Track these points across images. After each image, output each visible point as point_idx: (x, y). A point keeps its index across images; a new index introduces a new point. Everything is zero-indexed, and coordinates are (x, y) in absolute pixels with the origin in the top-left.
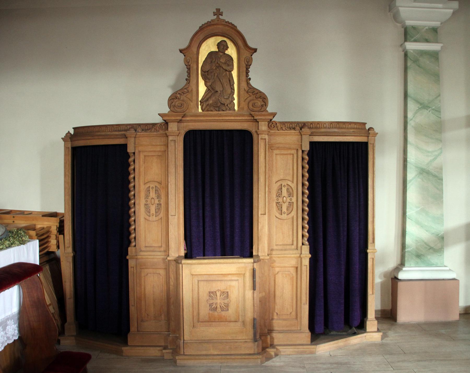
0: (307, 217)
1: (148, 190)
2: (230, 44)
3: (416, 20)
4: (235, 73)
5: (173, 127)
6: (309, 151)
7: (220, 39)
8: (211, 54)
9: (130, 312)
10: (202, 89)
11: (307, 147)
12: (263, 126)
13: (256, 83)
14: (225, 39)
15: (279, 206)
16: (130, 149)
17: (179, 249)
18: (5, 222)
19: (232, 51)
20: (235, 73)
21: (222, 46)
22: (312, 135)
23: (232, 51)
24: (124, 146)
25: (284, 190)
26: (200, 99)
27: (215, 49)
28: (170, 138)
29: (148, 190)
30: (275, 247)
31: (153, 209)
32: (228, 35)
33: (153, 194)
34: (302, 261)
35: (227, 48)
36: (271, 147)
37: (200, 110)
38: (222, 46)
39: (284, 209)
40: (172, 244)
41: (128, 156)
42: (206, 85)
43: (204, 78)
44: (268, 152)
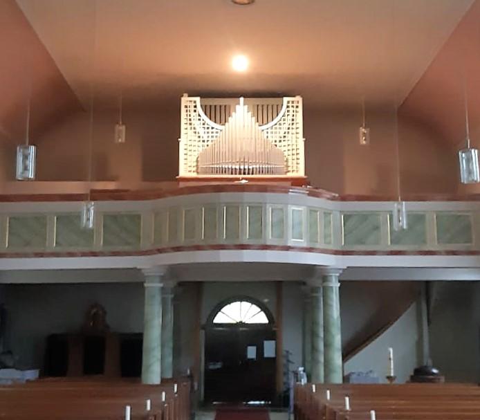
23: (101, 312)
34: (359, 252)
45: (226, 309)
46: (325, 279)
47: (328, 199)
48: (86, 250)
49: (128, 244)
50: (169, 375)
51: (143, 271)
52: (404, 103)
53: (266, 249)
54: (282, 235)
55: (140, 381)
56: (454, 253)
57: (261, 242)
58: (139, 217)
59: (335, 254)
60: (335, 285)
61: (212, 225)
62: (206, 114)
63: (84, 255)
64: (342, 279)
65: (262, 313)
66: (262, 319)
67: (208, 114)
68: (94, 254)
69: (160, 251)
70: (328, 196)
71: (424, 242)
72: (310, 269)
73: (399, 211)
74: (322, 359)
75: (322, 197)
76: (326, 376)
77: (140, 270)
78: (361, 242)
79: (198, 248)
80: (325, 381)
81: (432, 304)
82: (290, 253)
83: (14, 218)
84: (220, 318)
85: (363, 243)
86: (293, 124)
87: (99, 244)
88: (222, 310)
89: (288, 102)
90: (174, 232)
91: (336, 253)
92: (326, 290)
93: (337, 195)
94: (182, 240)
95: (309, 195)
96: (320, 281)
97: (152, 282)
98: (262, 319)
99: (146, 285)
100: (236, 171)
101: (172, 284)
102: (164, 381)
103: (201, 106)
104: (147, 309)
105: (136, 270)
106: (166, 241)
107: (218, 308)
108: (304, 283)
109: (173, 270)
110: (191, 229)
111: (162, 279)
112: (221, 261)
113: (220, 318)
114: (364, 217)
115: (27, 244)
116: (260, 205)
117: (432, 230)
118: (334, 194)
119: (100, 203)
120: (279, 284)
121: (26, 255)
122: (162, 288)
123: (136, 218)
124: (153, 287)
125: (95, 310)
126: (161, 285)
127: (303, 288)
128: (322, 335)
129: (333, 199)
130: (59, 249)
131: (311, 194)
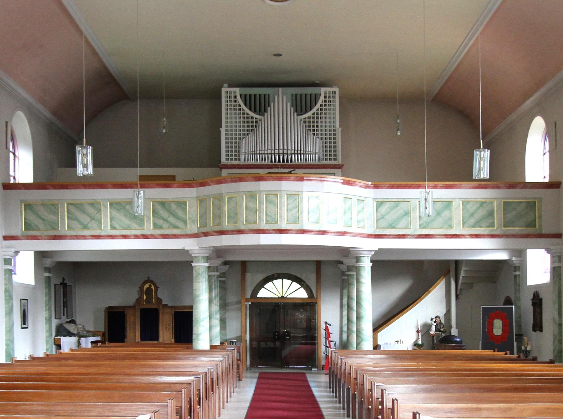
1: (166, 324)
2: (152, 285)
4: (153, 293)
5: (137, 307)
7: (150, 284)
8: (147, 288)
9: (140, 327)
10: (145, 297)
12: (161, 307)
13: (159, 296)
16: (126, 313)
18: (322, 298)
19: (153, 287)
20: (153, 293)
21: (150, 286)
22: (175, 309)
23: (153, 287)
24: (124, 312)
27: (148, 287)
29: (166, 324)
31: (132, 329)
33: (131, 325)
35: (151, 286)
38: (150, 286)
39: (167, 329)
40: (137, 338)
41: (125, 315)
43: (145, 294)
45: (269, 285)
46: (358, 259)
47: (361, 187)
49: (177, 227)
51: (190, 252)
53: (556, 234)
56: (477, 236)
57: (276, 227)
58: (185, 203)
60: (366, 265)
61: (253, 211)
62: (245, 105)
63: (136, 237)
64: (374, 259)
65: (294, 283)
66: (302, 294)
68: (145, 237)
69: (206, 234)
70: (361, 184)
71: (451, 227)
72: (345, 252)
73: (426, 199)
75: (357, 185)
76: (358, 344)
78: (392, 227)
79: (240, 232)
80: (357, 349)
81: (460, 281)
82: (283, 236)
83: (72, 204)
84: (263, 294)
85: (393, 228)
87: (149, 228)
90: (218, 217)
91: (370, 236)
92: (358, 269)
93: (370, 183)
95: (343, 183)
96: (355, 260)
97: (198, 261)
98: (302, 294)
99: (193, 264)
100: (327, 109)
101: (217, 262)
103: (241, 95)
104: (196, 285)
105: (183, 252)
106: (211, 225)
107: (261, 285)
109: (219, 252)
110: (234, 216)
111: (207, 259)
113: (263, 294)
114: (397, 203)
115: (85, 227)
116: (297, 193)
117: (457, 214)
118: (367, 183)
119: (147, 190)
120: (318, 264)
121: (84, 237)
123: (182, 204)
124: (200, 266)
125: (147, 286)
127: (341, 266)
128: (355, 308)
129: (367, 187)
130: (114, 232)
131: (346, 183)
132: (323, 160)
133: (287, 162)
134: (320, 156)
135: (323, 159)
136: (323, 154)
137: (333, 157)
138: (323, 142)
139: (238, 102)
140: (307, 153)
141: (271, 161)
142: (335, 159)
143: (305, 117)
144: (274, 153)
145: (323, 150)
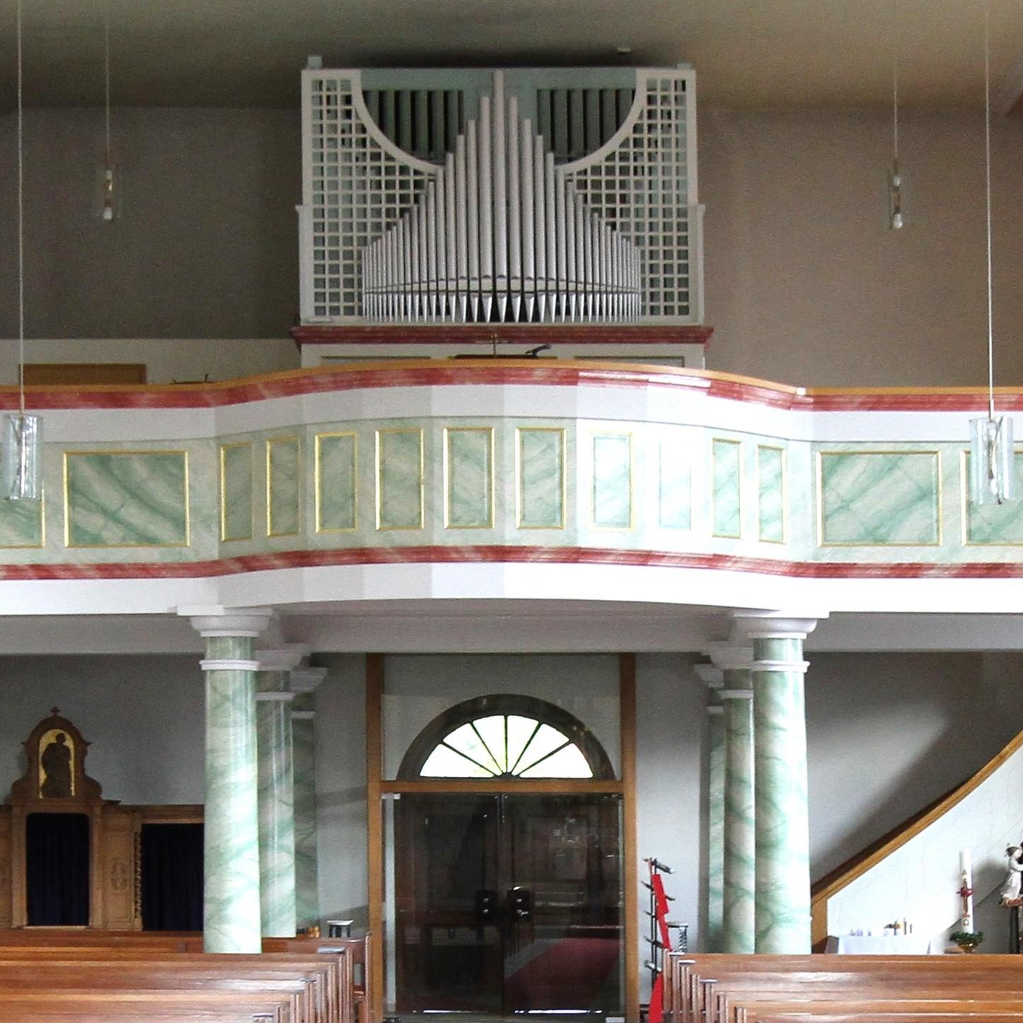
0: (139, 893)
2: (68, 737)
3: (97, 960)
4: (72, 763)
5: (16, 811)
6: (142, 833)
7: (59, 731)
8: (51, 746)
10: (43, 776)
11: (139, 830)
12: (97, 811)
13: (91, 773)
14: (63, 732)
15: (114, 881)
17: (22, 921)
19: (69, 743)
20: (72, 763)
21: (61, 738)
22: (144, 817)
23: (69, 743)
25: (119, 867)
26: (41, 785)
27: (53, 740)
28: (14, 820)
30: (111, 920)
32: (623, 824)
34: (508, 131)
35: (64, 740)
36: (105, 828)
37: (41, 797)
38: (61, 738)
42: (46, 772)
43: (44, 767)
44: (567, 499)
45: (461, 736)
46: (761, 648)
47: (772, 403)
48: (22, 558)
49: (150, 541)
50: (286, 929)
52: (770, 672)
54: (554, 516)
55: (198, 947)
58: (177, 459)
59: (796, 575)
62: (382, 126)
64: (816, 647)
67: (392, 134)
68: (43, 572)
69: (248, 564)
73: (990, 445)
74: (750, 884)
75: (757, 398)
76: (762, 934)
77: (187, 619)
78: (875, 537)
79: (364, 556)
85: (880, 541)
86: (651, 128)
88: (447, 740)
89: (651, 88)
91: (800, 570)
92: (760, 683)
93: (801, 391)
94: (317, 532)
96: (750, 652)
99: (206, 665)
102: (271, 946)
103: (366, 94)
104: (213, 736)
108: (706, 660)
111: (254, 647)
112: (437, 594)
118: (791, 389)
120: (627, 663)
122: (258, 675)
126: (252, 666)
127: (704, 672)
128: (751, 813)
129: (793, 404)
132: (644, 313)
133: (521, 320)
134: (635, 300)
135: (644, 308)
136: (643, 294)
137: (676, 303)
138: (643, 252)
139: (357, 117)
140: (562, 286)
141: (470, 317)
142: (684, 311)
143: (582, 168)
144: (477, 288)
145: (643, 280)
